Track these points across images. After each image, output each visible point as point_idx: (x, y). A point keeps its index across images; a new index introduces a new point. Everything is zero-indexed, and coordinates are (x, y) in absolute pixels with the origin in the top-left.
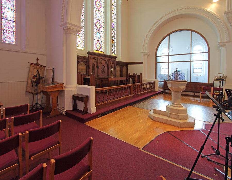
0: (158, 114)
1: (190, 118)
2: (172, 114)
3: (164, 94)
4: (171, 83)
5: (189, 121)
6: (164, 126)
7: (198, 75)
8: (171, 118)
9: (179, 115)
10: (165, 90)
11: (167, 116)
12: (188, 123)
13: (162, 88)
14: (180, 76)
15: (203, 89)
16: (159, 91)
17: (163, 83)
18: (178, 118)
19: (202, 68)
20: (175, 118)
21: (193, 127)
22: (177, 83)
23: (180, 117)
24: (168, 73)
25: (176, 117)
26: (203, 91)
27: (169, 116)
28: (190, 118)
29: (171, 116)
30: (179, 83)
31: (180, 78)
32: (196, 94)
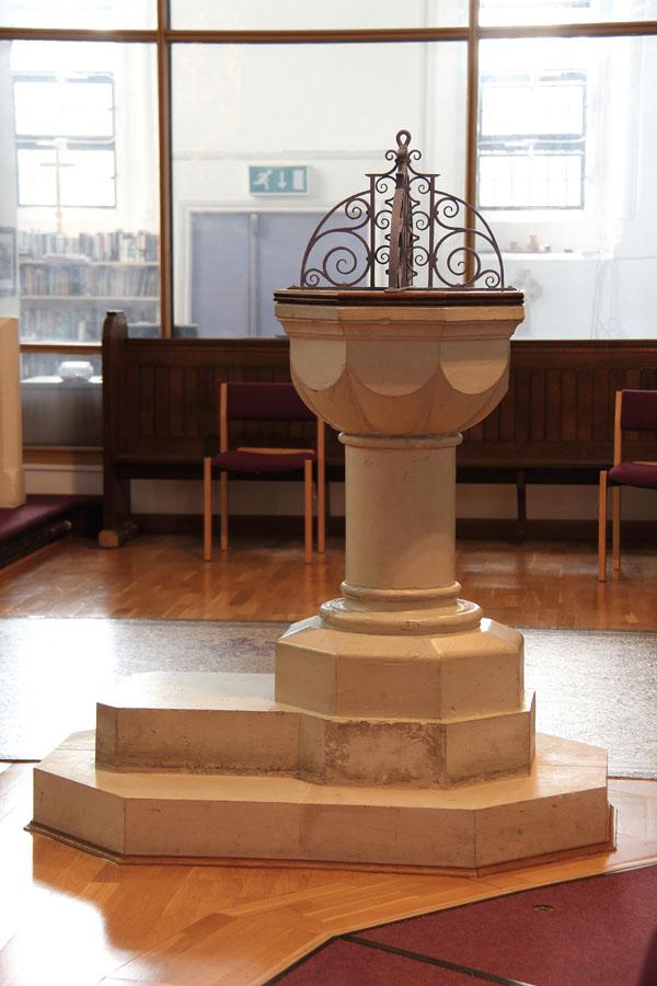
0: (175, 768)
1: (553, 757)
2: (363, 726)
3: (109, 537)
4: (342, 323)
5: (554, 778)
6: (284, 892)
7: (534, 249)
8: (357, 779)
9: (442, 729)
10: (120, 472)
11: (303, 769)
12: (556, 803)
13: (79, 457)
14: (440, 232)
15: (624, 428)
16: (33, 500)
17: (86, 371)
18: (439, 769)
19: (590, 141)
20: (399, 779)
21: (606, 846)
22: (414, 323)
23: (457, 753)
24: (155, 229)
25: (414, 755)
26: (624, 458)
27: (321, 759)
28: (553, 757)
29: (359, 753)
30: (444, 324)
31: (441, 264)
32: (548, 502)
